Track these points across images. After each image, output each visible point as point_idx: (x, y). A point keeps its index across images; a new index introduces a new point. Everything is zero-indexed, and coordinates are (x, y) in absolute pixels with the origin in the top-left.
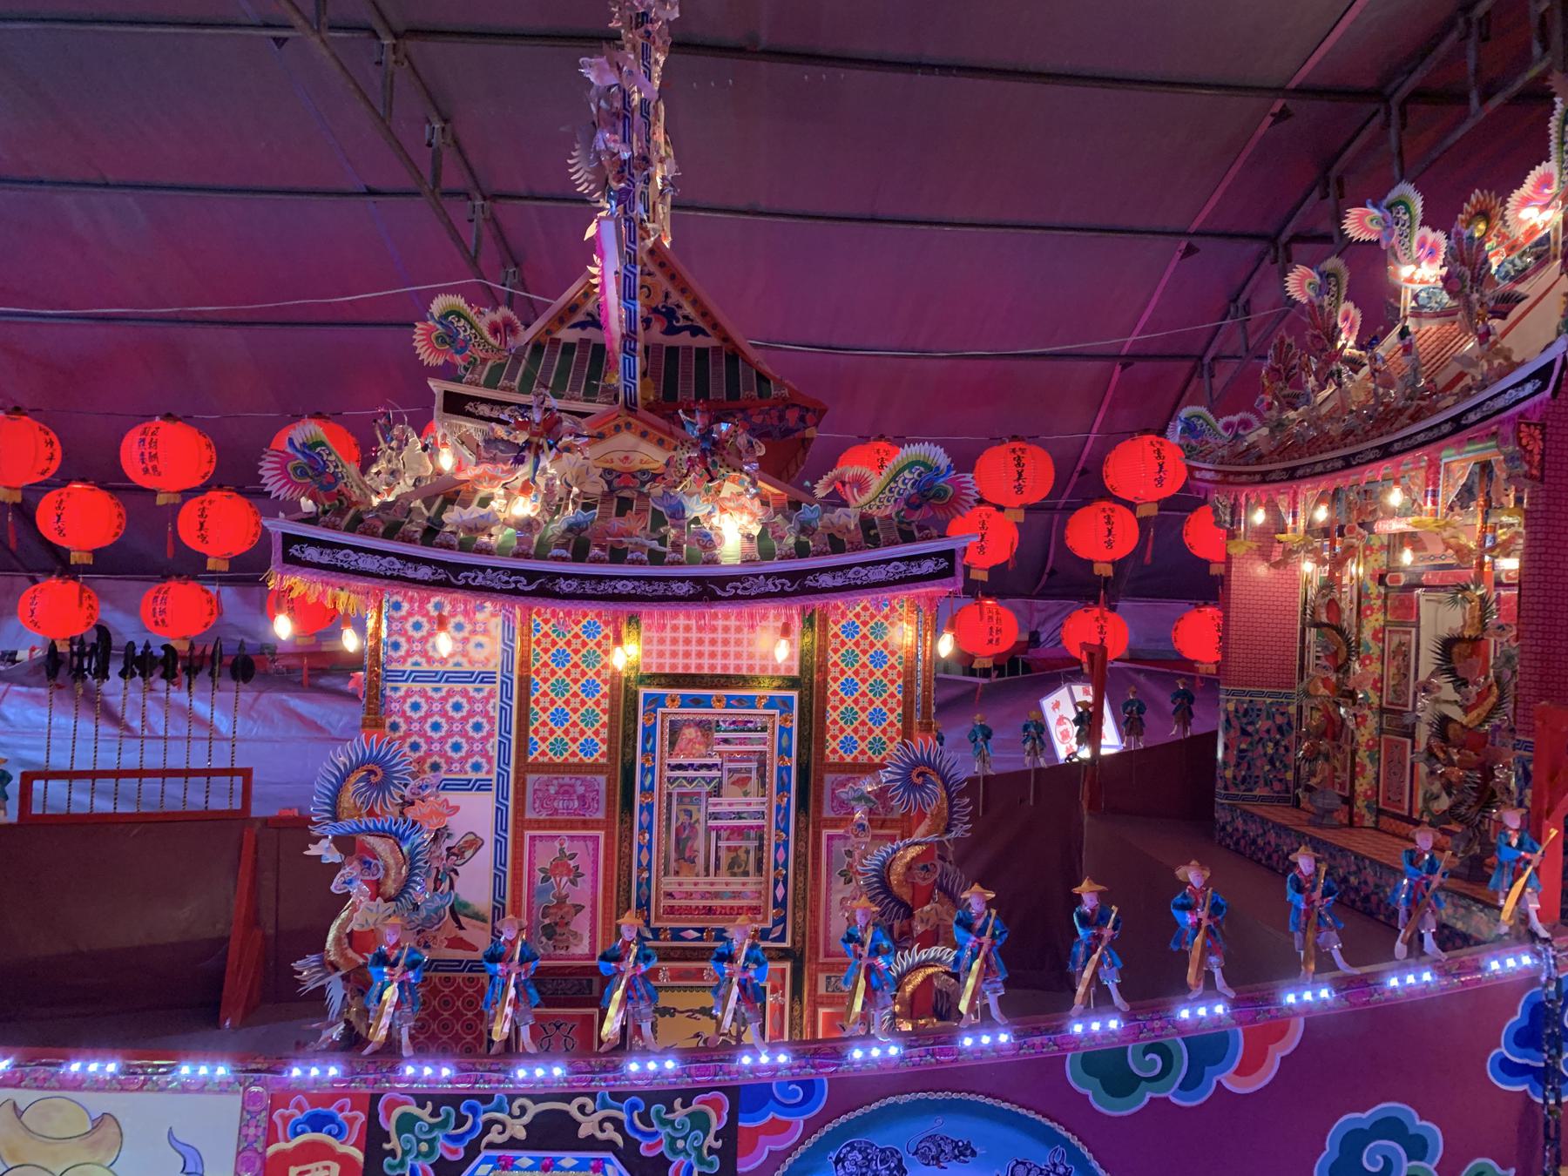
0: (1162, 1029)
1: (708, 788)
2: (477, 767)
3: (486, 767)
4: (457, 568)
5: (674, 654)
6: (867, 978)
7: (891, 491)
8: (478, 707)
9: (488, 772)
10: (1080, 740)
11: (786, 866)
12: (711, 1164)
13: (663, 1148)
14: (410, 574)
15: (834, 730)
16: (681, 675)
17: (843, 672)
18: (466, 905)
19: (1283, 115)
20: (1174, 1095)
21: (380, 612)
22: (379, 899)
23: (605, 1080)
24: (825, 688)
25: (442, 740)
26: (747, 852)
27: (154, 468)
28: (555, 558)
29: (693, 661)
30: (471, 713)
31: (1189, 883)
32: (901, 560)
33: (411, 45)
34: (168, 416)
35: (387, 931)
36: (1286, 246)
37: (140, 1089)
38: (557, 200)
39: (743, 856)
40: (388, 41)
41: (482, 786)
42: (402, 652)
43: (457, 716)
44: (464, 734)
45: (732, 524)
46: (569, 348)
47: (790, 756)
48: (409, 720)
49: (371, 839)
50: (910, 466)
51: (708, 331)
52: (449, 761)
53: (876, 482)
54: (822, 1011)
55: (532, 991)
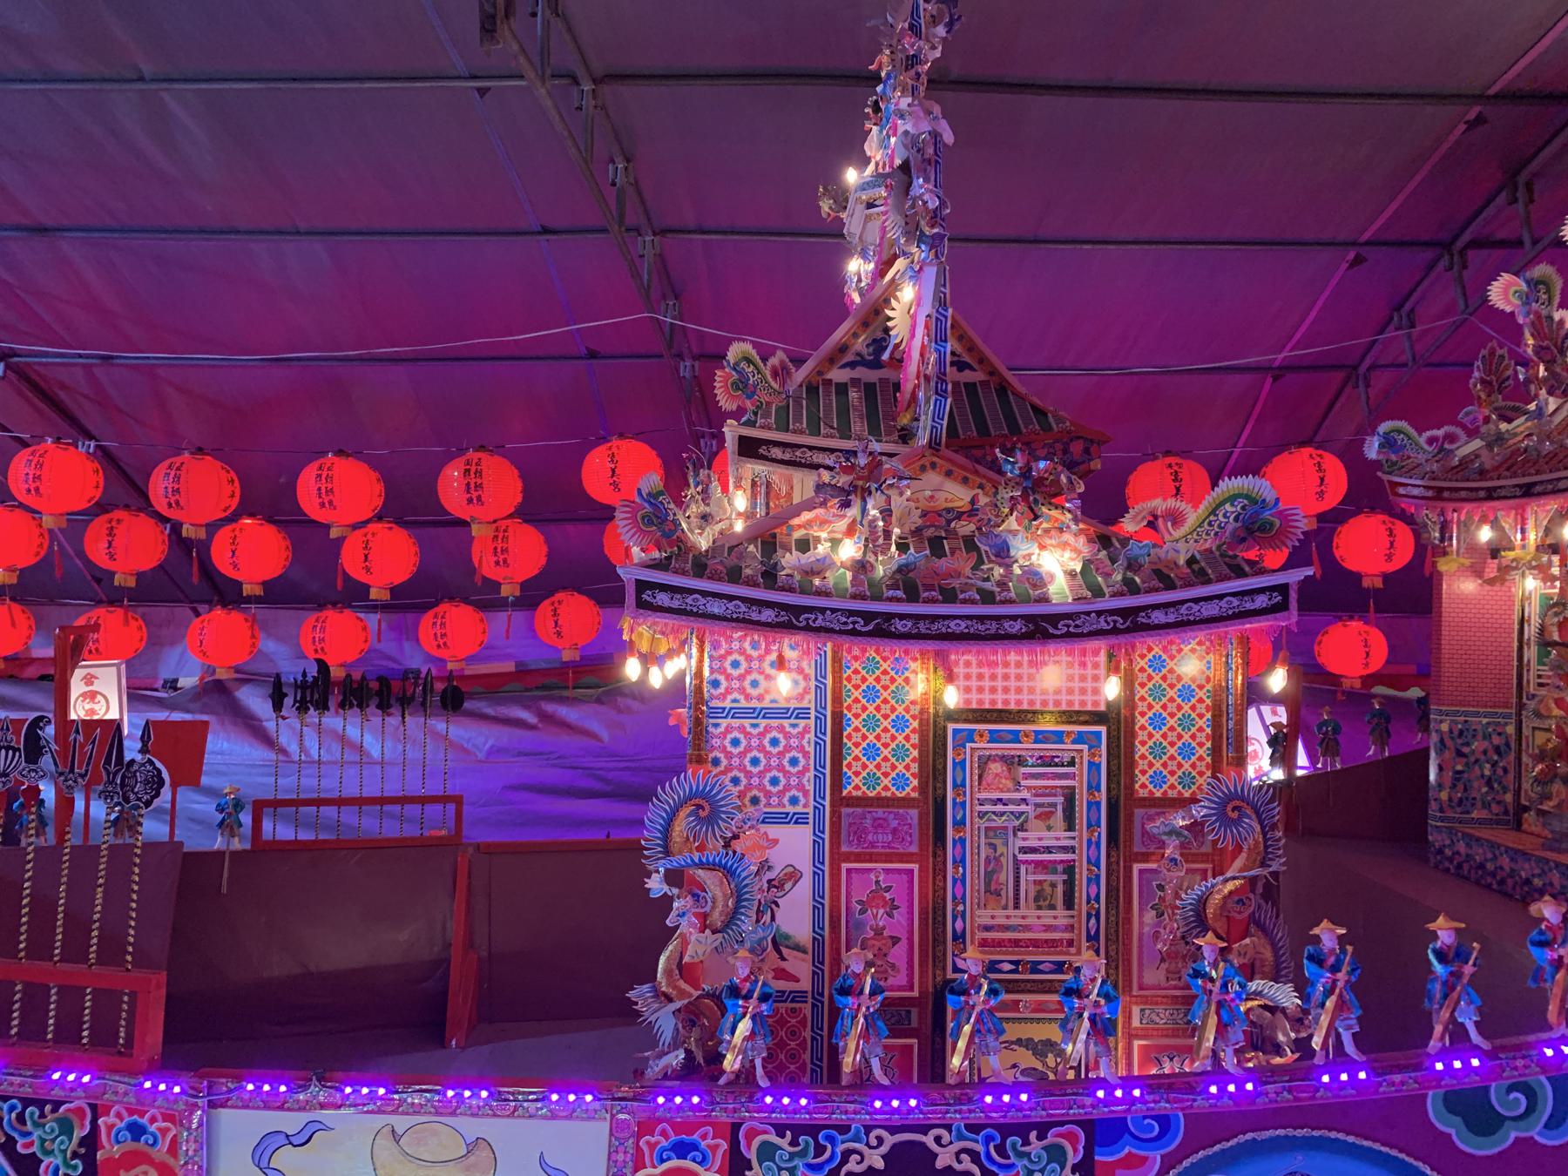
0: (1525, 1067)
1: (1017, 823)
2: (794, 801)
3: (803, 801)
4: (798, 610)
5: (980, 690)
6: (1218, 1013)
7: (1210, 524)
8: (794, 742)
9: (805, 806)
10: (1274, 761)
11: (1097, 899)
12: (75, 1168)
13: (35, 1149)
14: (755, 616)
15: (1142, 765)
16: (988, 711)
17: (1150, 707)
18: (787, 937)
19: (1480, 120)
20: (1540, 1134)
21: (701, 651)
22: (708, 931)
23: (960, 1112)
24: (1133, 723)
25: (761, 775)
26: (1053, 885)
27: (330, 502)
28: (890, 599)
29: (1000, 697)
30: (788, 748)
31: (1543, 919)
32: (1234, 595)
33: (606, 89)
34: (340, 453)
35: (739, 964)
36: (1462, 252)
37: (512, 1115)
38: (725, 233)
39: (1048, 889)
40: (587, 87)
41: (800, 820)
42: (722, 690)
43: (775, 751)
44: (781, 768)
45: (1054, 559)
46: (842, 389)
47: (1099, 791)
48: (729, 756)
49: (700, 872)
50: (1232, 499)
51: (976, 366)
52: (768, 795)
53: (1192, 517)
54: (1137, 1043)
55: (880, 1024)
